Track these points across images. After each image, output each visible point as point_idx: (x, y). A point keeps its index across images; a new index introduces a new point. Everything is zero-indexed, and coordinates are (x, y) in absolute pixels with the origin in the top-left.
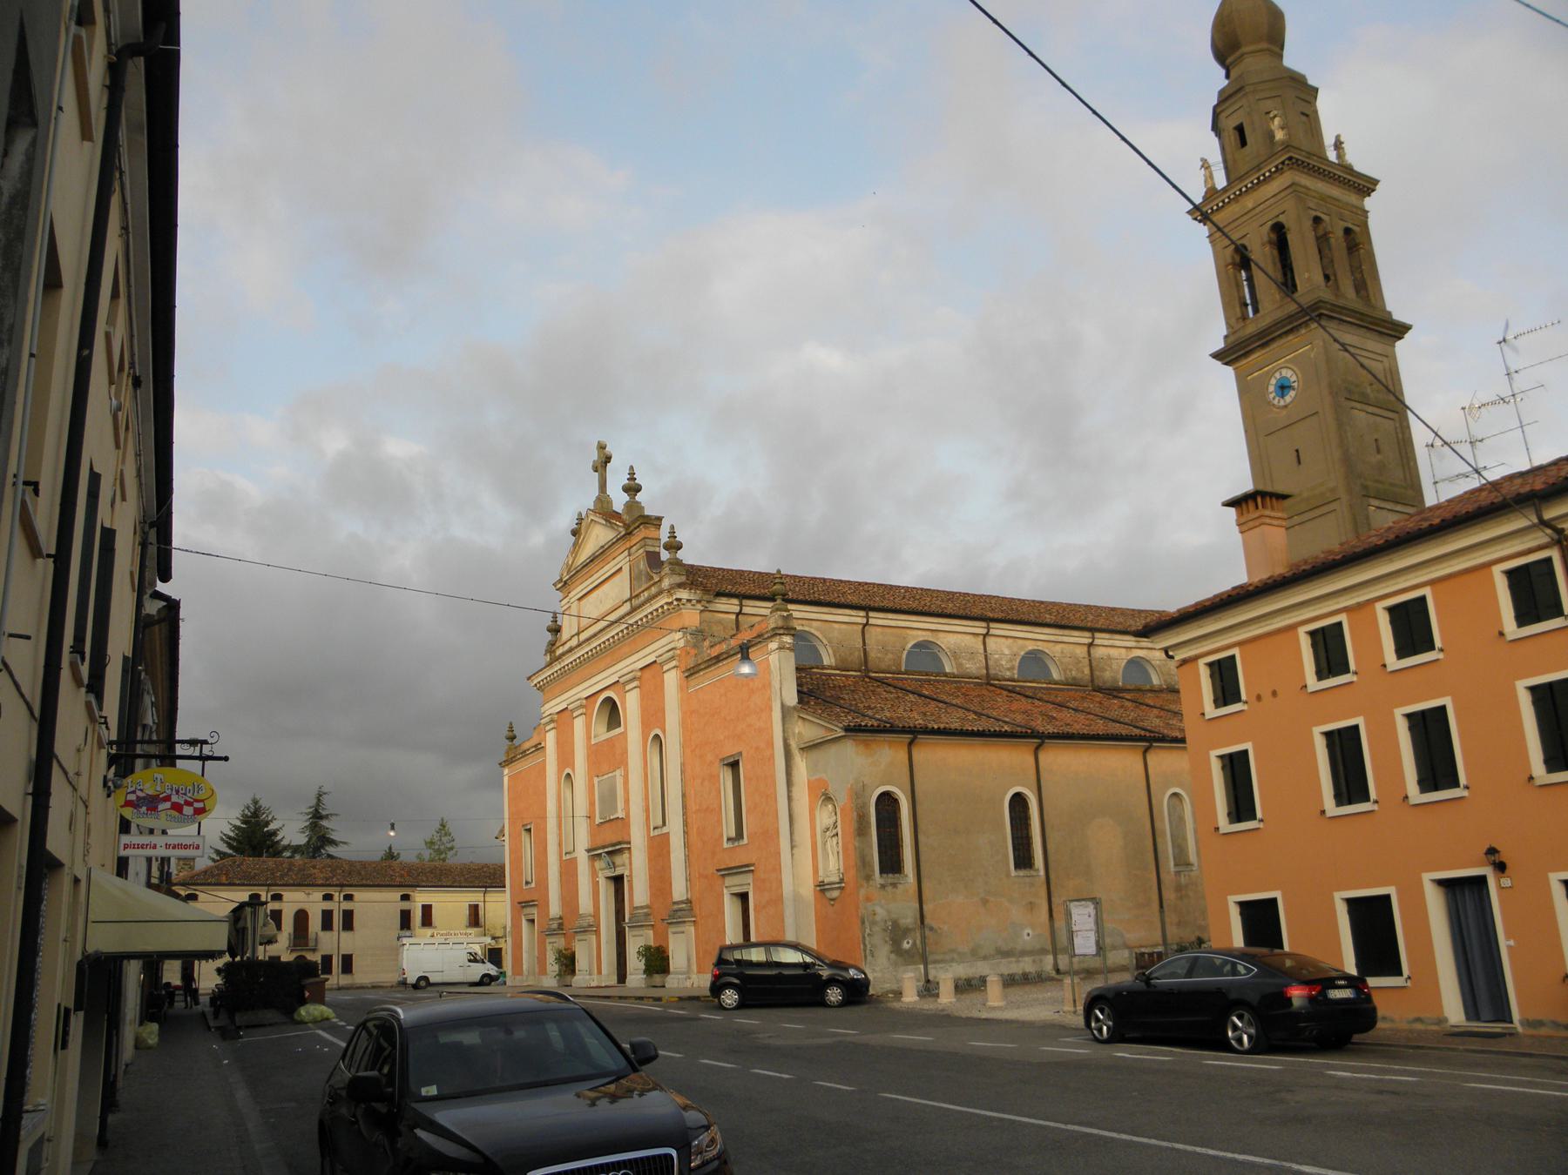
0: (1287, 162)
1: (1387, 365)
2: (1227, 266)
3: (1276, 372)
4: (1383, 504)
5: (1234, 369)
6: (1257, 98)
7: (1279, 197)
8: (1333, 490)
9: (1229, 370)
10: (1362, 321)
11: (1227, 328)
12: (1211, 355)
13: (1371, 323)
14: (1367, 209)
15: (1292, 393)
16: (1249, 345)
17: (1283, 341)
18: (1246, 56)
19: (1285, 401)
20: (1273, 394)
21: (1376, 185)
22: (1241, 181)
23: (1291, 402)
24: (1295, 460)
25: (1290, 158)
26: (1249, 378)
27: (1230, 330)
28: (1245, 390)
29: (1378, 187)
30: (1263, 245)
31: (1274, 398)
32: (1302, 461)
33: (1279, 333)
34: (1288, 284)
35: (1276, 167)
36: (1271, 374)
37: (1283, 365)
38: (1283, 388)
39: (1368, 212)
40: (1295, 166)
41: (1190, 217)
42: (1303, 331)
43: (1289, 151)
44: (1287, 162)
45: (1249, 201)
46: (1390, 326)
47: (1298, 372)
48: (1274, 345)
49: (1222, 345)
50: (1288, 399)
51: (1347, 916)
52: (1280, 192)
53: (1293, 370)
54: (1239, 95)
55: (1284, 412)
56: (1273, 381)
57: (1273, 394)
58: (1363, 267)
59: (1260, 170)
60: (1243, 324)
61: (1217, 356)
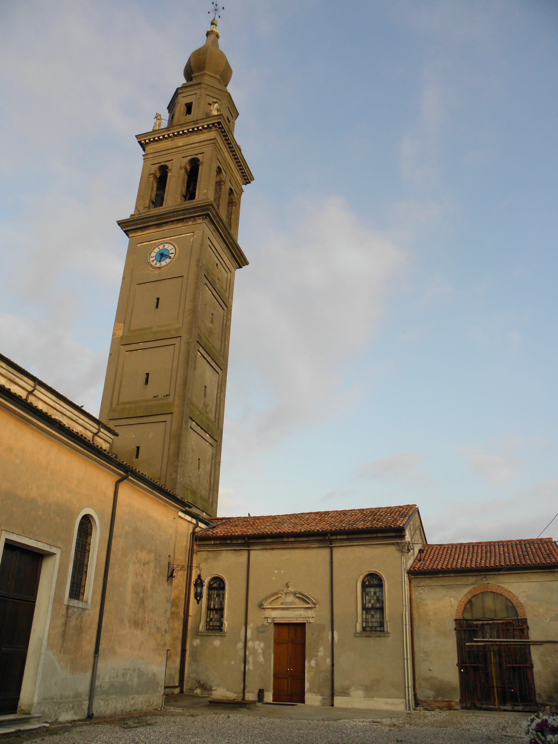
1: (229, 277)
2: (150, 175)
3: (161, 244)
4: (206, 356)
6: (207, 93)
7: (202, 144)
8: (177, 330)
10: (227, 237)
12: (117, 222)
13: (231, 244)
15: (168, 260)
16: (148, 222)
18: (206, 75)
22: (181, 127)
23: (165, 266)
24: (155, 304)
25: (219, 123)
27: (138, 212)
28: (131, 252)
30: (181, 168)
31: (153, 261)
34: (190, 194)
35: (208, 125)
38: (162, 255)
40: (220, 130)
41: (136, 140)
42: (190, 223)
43: (220, 118)
44: (216, 124)
45: (180, 142)
46: (239, 255)
48: (165, 228)
49: (129, 217)
50: (163, 263)
51: (23, 368)
52: (205, 141)
53: (174, 246)
55: (157, 272)
56: (157, 250)
58: (232, 216)
59: (197, 124)
60: (147, 210)
61: (121, 224)
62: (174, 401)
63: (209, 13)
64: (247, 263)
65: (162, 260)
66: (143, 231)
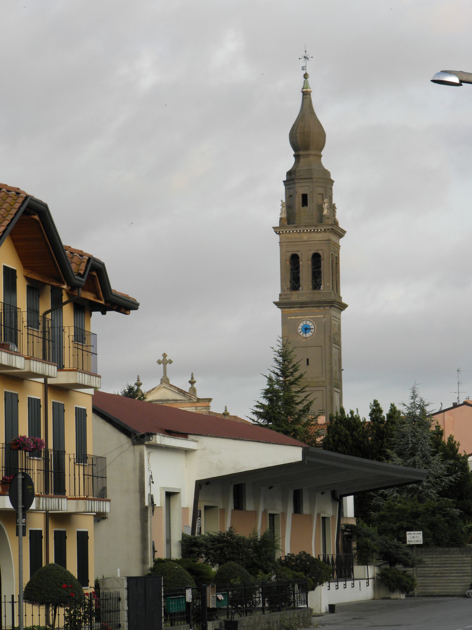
0: (330, 230)
5: (281, 311)
9: (280, 310)
11: (281, 291)
14: (340, 245)
16: (294, 305)
17: (310, 309)
18: (311, 156)
19: (306, 336)
20: (301, 330)
21: (345, 234)
26: (289, 318)
27: (283, 292)
29: (345, 235)
32: (306, 360)
33: (310, 305)
36: (300, 321)
37: (308, 319)
38: (306, 329)
39: (340, 246)
41: (273, 230)
42: (322, 308)
44: (330, 230)
47: (315, 325)
50: (308, 335)
53: (313, 323)
54: (309, 180)
55: (305, 340)
56: (302, 324)
57: (301, 330)
62: (418, 596)
63: (300, 59)
64: (346, 232)
65: (307, 332)
66: (290, 309)
